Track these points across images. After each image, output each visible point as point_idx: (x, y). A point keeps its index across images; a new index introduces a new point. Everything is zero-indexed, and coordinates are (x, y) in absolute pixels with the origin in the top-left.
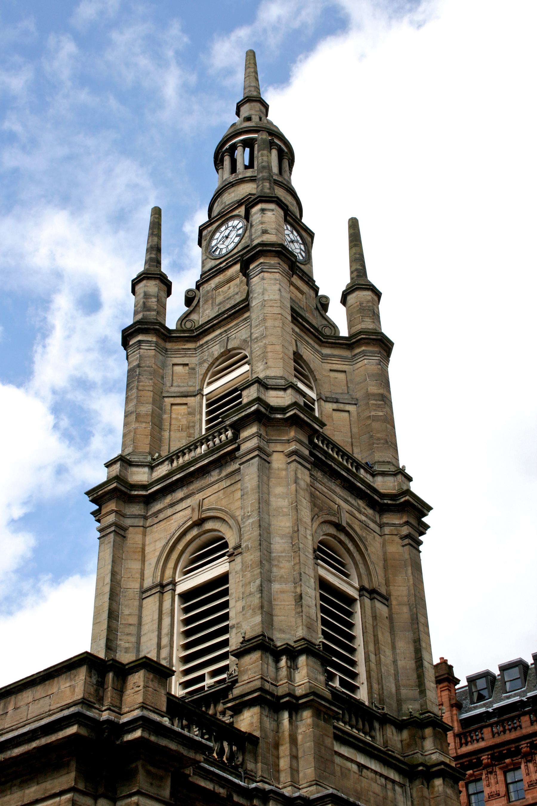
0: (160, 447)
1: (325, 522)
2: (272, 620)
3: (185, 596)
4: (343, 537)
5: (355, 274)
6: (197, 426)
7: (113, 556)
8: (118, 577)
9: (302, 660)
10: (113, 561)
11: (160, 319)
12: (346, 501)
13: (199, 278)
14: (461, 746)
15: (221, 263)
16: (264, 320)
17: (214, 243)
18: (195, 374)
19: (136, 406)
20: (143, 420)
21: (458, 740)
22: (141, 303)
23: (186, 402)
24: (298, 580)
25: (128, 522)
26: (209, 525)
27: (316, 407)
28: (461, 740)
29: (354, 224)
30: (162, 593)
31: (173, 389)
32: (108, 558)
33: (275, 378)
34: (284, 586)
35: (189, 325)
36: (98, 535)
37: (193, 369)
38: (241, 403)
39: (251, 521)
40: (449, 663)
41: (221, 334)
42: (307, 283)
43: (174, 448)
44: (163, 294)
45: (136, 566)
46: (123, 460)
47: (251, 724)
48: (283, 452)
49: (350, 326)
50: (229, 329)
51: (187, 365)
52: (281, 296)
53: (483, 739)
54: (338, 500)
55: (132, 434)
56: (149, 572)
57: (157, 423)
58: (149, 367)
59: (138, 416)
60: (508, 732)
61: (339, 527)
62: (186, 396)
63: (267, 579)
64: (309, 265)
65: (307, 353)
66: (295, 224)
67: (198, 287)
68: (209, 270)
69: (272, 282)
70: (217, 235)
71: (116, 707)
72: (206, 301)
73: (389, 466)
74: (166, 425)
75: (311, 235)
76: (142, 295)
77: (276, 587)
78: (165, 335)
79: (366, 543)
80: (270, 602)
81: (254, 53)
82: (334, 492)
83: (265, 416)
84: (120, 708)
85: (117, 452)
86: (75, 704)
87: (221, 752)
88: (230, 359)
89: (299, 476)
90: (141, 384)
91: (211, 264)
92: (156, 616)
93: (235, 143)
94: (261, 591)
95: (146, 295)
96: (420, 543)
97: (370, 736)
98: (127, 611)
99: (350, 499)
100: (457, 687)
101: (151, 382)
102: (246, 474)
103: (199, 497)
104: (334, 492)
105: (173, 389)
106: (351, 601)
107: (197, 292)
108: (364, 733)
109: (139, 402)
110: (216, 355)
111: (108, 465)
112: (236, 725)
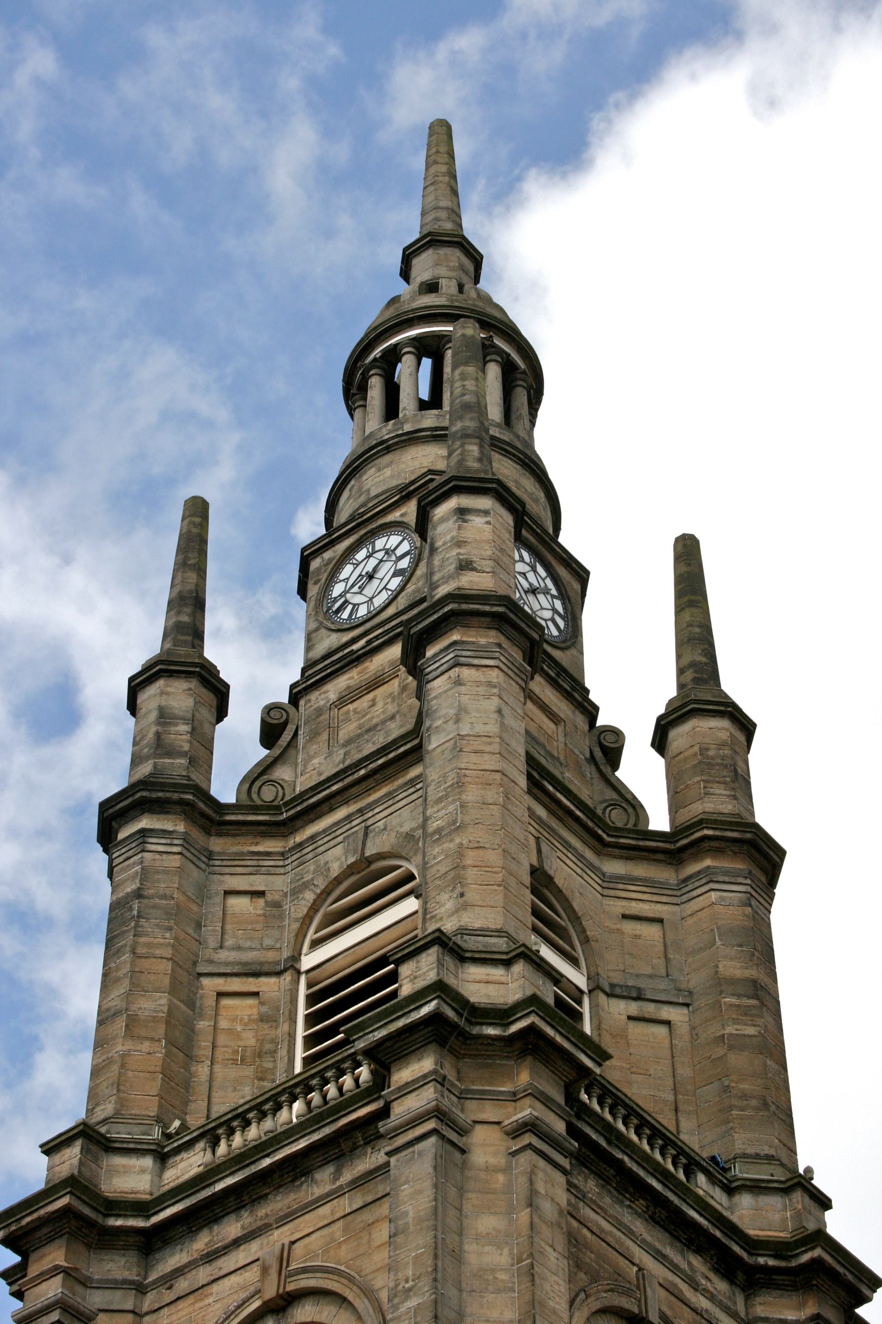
0: (186, 1103)
5: (689, 675)
6: (283, 1052)
12: (660, 1257)
15: (354, 641)
16: (459, 785)
18: (281, 917)
20: (143, 1033)
22: (151, 735)
23: (256, 990)
29: (687, 551)
31: (223, 955)
35: (268, 794)
37: (277, 905)
39: (413, 1302)
41: (349, 818)
42: (568, 696)
43: (220, 1108)
44: (206, 714)
48: (499, 1123)
49: (675, 806)
50: (370, 806)
51: (261, 894)
55: (115, 1068)
58: (164, 897)
59: (132, 1021)
65: (565, 872)
66: (540, 547)
68: (325, 657)
73: (771, 1169)
75: (582, 575)
76: (154, 715)
78: (209, 816)
82: (629, 1233)
83: (453, 1030)
89: (541, 1187)
90: (143, 940)
91: (329, 641)
93: (396, 345)
95: (165, 717)
99: (668, 1251)
101: (168, 935)
102: (403, 1179)
103: (280, 1236)
104: (629, 1233)
105: (223, 955)
107: (292, 710)
110: (336, 869)
111: (50, 1149)
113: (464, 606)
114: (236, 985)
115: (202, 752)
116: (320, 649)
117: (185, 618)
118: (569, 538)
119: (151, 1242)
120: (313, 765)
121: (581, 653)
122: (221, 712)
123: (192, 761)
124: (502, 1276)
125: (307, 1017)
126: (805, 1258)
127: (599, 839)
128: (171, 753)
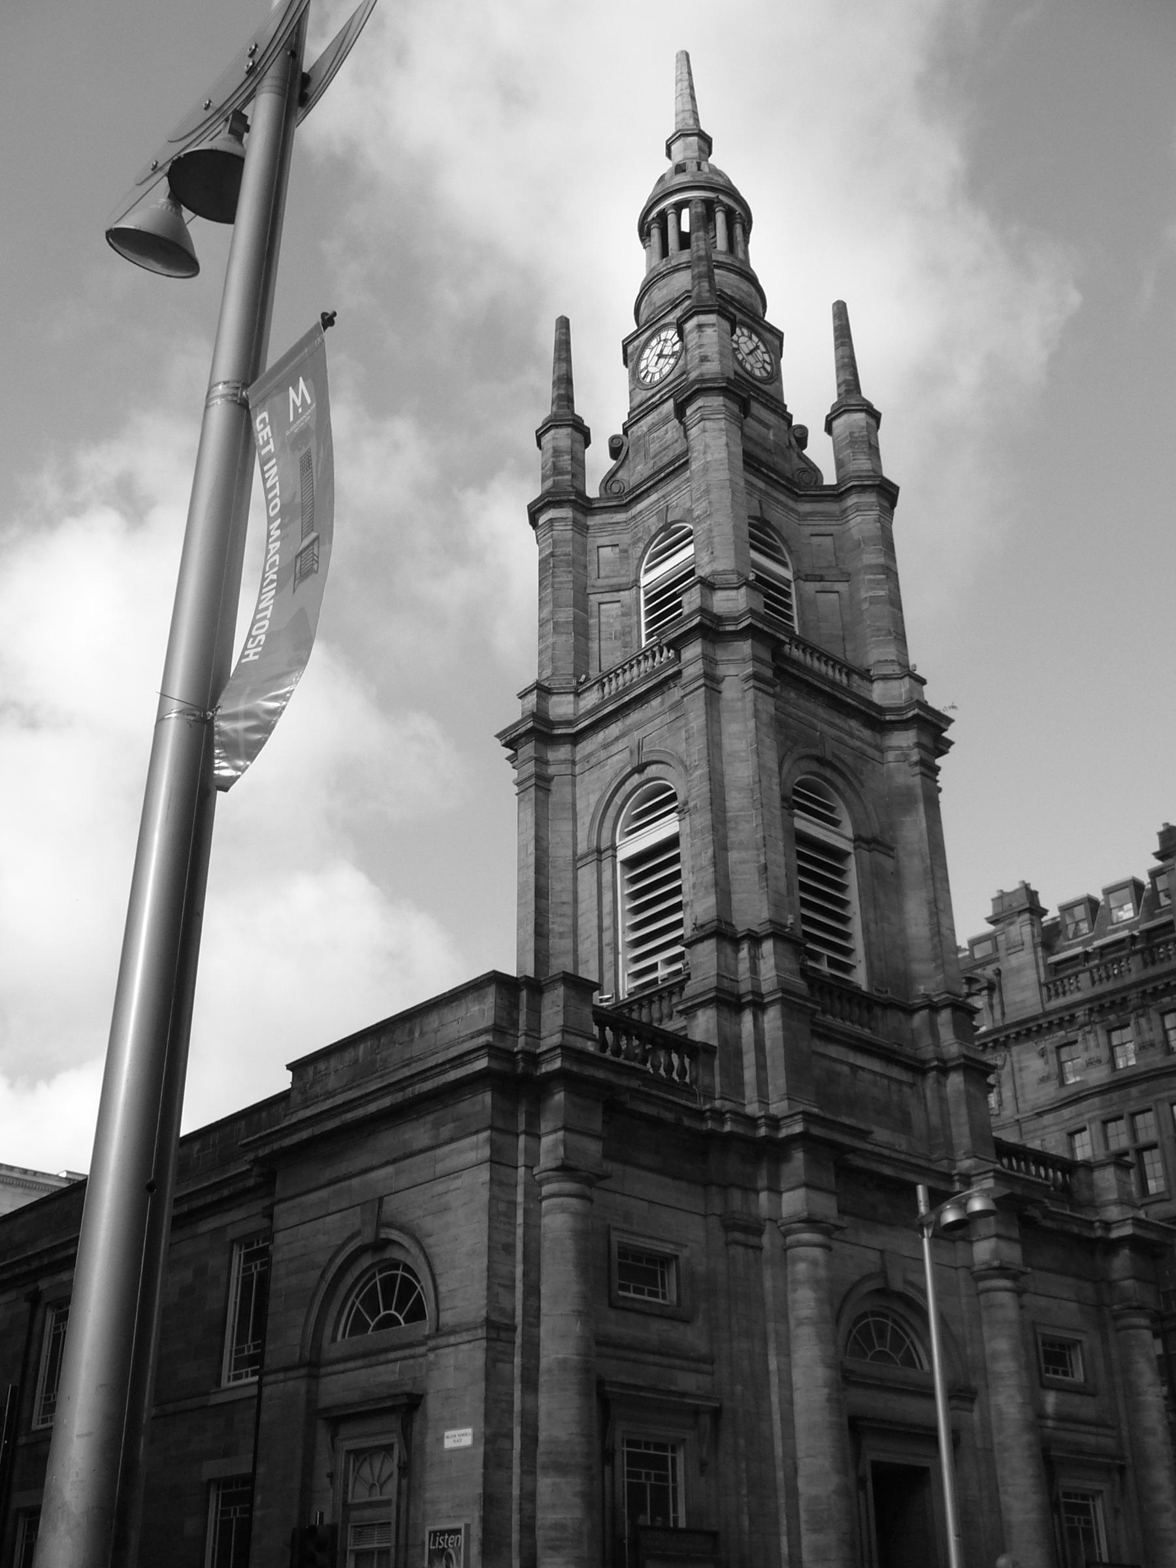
0: (588, 664)
1: (802, 758)
2: (730, 899)
3: (632, 862)
4: (828, 773)
5: (843, 388)
6: (635, 632)
7: (536, 818)
8: (544, 844)
9: (768, 946)
10: (536, 824)
11: (577, 483)
12: (832, 725)
13: (626, 419)
14: (1050, 998)
15: (653, 396)
16: (707, 491)
17: (643, 365)
18: (628, 558)
19: (553, 613)
20: (562, 630)
21: (1044, 990)
22: (550, 464)
24: (762, 845)
25: (552, 770)
26: (652, 771)
27: (793, 591)
28: (1049, 989)
29: (840, 310)
30: (600, 860)
31: (600, 582)
32: (530, 820)
33: (724, 572)
34: (744, 855)
35: (616, 488)
36: (516, 789)
37: (626, 551)
38: (680, 614)
39: (698, 773)
40: (1033, 888)
41: (658, 500)
42: (774, 411)
43: (605, 667)
44: (578, 447)
45: (566, 827)
46: (542, 690)
47: (707, 1031)
49: (840, 465)
50: (669, 494)
52: (730, 453)
53: (1079, 989)
54: (820, 725)
55: (550, 651)
56: (582, 835)
57: (582, 630)
58: (565, 555)
59: (556, 624)
60: (1112, 978)
61: (821, 761)
62: (619, 591)
63: (721, 847)
64: (777, 383)
65: (776, 516)
66: (754, 324)
67: (625, 431)
68: (639, 406)
69: (716, 433)
70: (647, 351)
71: (533, 1030)
72: (637, 452)
73: (892, 667)
74: (594, 632)
75: (779, 336)
76: (551, 452)
77: (733, 856)
78: (585, 506)
79: (862, 777)
80: (727, 876)
81: (687, 55)
82: (815, 715)
83: (711, 630)
84: (539, 1032)
85: (531, 678)
86: (484, 1031)
87: (669, 1068)
88: (672, 536)
89: (760, 707)
90: (557, 580)
91: (642, 395)
92: (595, 892)
94: (715, 865)
95: (557, 452)
96: (937, 770)
97: (870, 1028)
98: (559, 887)
99: (837, 721)
100: (1044, 919)
103: (637, 735)
104: (815, 715)
105: (600, 582)
106: (841, 855)
107: (624, 438)
108: (861, 1025)
109: (556, 605)
110: (654, 530)
111: (522, 696)
112: (690, 1037)
113: (704, 386)
114: (608, 597)
115: (579, 469)
116: (637, 401)
117: (562, 392)
118: (772, 317)
119: (575, 739)
120: (637, 471)
121: (781, 383)
122: (587, 442)
123: (573, 476)
124: (743, 754)
125: (646, 612)
126: (910, 714)
127: (796, 494)
128: (561, 473)
